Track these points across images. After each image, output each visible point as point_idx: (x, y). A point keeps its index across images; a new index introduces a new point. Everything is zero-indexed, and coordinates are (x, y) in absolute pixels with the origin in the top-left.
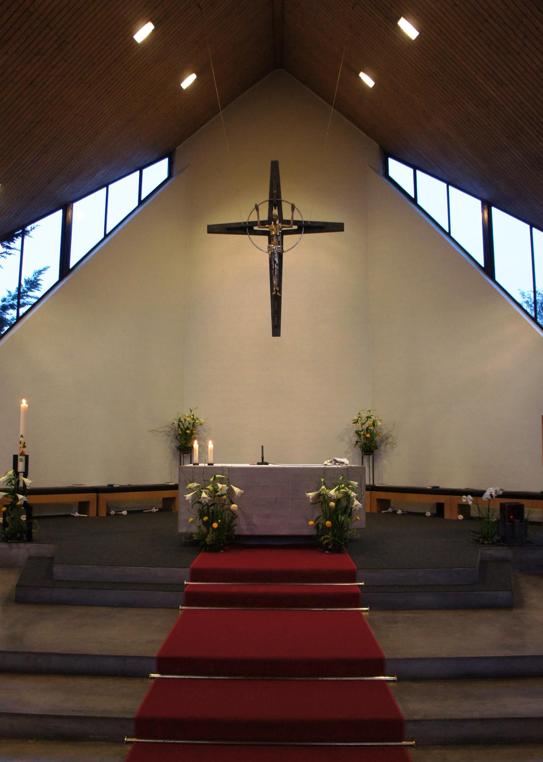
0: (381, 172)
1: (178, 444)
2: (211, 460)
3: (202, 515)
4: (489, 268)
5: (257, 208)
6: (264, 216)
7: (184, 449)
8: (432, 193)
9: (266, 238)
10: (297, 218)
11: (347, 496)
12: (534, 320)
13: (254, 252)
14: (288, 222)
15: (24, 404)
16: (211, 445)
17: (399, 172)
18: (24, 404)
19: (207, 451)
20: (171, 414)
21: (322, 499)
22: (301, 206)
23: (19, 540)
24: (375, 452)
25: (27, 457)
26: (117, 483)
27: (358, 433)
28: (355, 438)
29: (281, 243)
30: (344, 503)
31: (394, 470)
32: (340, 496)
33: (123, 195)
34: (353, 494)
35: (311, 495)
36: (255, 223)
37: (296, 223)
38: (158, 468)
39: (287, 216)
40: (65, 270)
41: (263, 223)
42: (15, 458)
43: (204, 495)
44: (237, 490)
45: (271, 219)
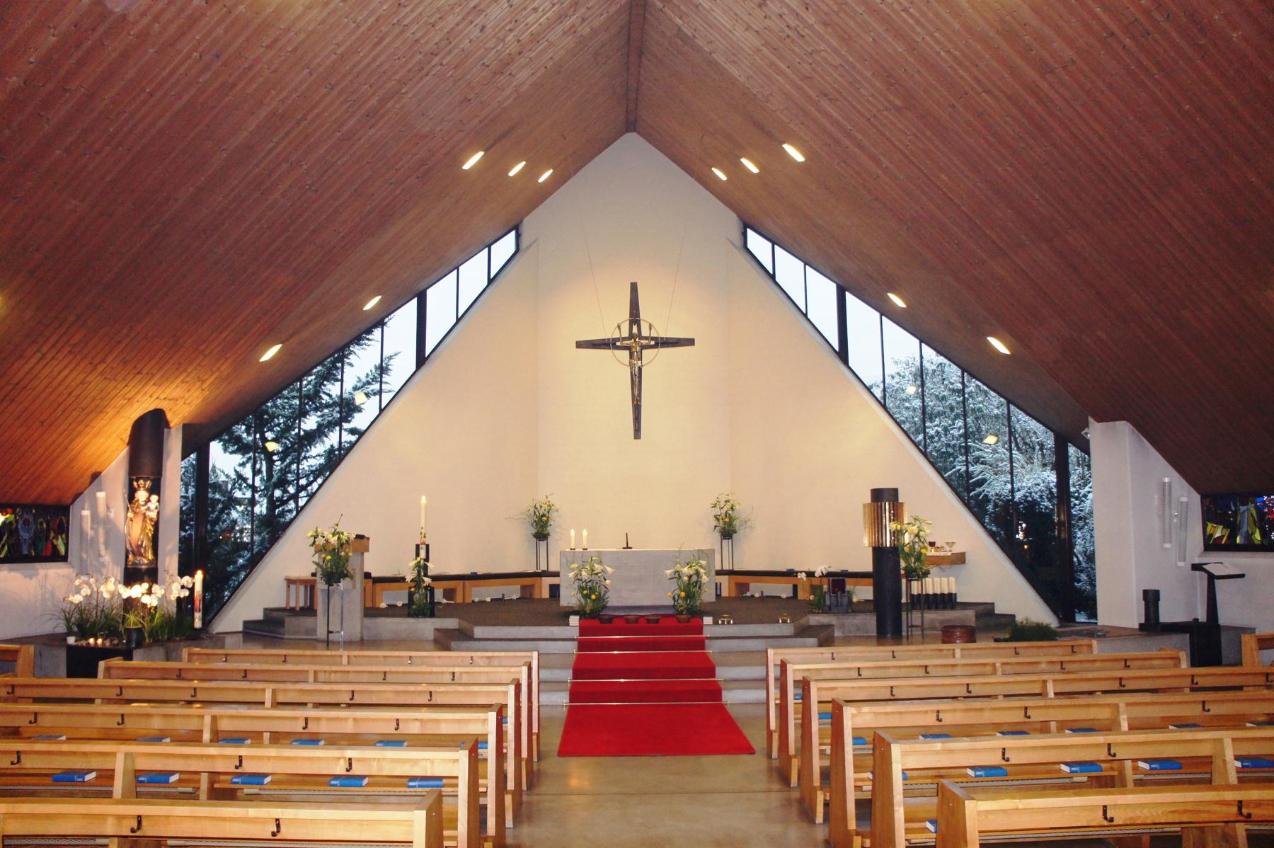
0: (739, 243)
1: (534, 531)
2: (585, 544)
3: (581, 589)
4: (843, 354)
5: (619, 327)
6: (625, 334)
7: (541, 535)
8: (789, 269)
9: (627, 352)
10: (654, 334)
11: (697, 573)
12: (884, 406)
13: (616, 363)
14: (646, 338)
15: (424, 500)
16: (585, 533)
17: (757, 244)
18: (424, 500)
19: (572, 536)
20: (526, 504)
21: (678, 575)
22: (656, 321)
23: (424, 615)
24: (734, 536)
25: (428, 546)
26: (480, 571)
27: (716, 517)
28: (715, 523)
29: (640, 358)
30: (694, 578)
31: (752, 554)
32: (692, 572)
33: (474, 273)
34: (702, 571)
35: (669, 572)
36: (618, 339)
37: (653, 339)
38: (515, 555)
39: (645, 333)
40: (421, 360)
41: (624, 339)
42: (418, 546)
43: (584, 573)
44: (609, 569)
45: (631, 336)
